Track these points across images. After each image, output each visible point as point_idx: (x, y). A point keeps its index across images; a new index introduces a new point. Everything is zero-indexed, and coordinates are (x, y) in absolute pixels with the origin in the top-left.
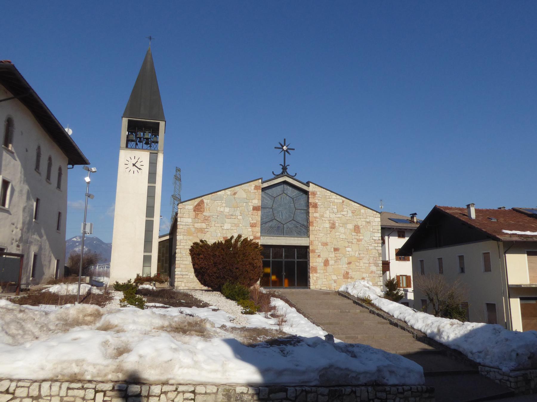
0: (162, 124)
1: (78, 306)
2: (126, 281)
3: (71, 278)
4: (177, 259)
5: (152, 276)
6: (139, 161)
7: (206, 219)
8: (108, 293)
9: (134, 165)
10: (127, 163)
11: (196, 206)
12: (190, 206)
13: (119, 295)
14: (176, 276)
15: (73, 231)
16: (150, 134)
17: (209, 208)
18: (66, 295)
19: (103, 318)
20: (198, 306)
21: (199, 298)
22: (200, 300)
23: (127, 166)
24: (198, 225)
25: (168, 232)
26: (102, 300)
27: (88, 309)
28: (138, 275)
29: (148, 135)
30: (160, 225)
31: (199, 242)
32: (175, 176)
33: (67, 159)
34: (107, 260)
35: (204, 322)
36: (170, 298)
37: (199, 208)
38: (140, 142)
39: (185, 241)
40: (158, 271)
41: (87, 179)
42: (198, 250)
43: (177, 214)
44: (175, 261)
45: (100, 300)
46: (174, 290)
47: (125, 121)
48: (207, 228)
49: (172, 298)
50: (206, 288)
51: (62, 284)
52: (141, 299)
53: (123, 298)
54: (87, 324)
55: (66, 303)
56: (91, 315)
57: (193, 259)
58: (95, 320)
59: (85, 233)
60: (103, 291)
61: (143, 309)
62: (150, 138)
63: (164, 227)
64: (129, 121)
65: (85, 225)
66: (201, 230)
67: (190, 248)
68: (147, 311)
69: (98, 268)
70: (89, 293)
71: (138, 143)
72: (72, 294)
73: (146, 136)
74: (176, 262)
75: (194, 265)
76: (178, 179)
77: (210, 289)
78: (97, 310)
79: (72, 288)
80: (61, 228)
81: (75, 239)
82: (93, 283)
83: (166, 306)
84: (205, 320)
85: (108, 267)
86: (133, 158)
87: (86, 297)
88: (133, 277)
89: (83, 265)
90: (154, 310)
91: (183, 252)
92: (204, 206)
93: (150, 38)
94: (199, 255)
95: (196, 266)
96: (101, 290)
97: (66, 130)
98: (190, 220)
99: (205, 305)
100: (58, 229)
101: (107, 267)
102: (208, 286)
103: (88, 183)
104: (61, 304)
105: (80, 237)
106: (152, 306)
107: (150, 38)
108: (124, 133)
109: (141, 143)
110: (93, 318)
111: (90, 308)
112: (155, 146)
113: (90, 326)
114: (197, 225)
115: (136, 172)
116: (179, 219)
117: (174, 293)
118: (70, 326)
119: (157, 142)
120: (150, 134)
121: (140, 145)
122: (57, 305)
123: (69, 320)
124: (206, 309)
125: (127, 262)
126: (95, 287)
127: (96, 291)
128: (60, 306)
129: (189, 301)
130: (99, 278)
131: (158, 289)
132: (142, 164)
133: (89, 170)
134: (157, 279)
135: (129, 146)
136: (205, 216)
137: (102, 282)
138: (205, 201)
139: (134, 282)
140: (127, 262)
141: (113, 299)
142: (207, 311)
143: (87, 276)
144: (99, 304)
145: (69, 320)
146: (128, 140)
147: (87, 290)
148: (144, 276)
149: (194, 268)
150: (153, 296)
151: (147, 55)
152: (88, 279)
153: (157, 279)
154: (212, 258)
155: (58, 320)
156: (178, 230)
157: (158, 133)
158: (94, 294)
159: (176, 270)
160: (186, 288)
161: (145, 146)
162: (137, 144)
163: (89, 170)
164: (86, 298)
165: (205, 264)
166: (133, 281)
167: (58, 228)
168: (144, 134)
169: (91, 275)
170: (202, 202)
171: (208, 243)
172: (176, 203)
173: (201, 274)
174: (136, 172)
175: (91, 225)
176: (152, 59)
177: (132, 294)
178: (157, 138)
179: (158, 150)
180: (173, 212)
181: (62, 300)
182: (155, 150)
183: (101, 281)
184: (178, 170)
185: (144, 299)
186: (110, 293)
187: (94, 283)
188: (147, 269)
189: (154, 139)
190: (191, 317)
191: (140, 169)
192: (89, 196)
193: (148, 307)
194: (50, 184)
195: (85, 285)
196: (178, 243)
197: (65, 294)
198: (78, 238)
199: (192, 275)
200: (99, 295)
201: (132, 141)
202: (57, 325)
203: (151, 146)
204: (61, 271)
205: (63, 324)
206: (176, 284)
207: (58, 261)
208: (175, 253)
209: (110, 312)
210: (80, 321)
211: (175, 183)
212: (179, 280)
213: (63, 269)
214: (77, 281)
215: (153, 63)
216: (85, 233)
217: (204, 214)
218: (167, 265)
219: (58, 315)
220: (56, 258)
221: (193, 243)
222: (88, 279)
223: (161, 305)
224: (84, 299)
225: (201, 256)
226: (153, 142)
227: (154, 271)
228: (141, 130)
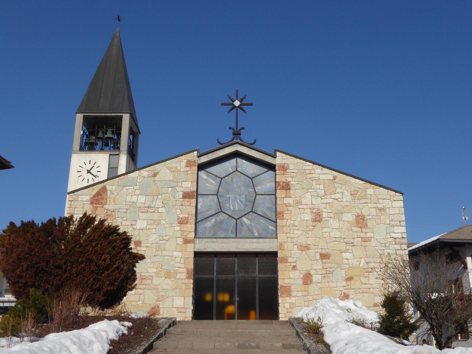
6: (95, 166)
9: (89, 172)
10: (80, 169)
11: (95, 196)
17: (115, 198)
23: (80, 174)
47: (79, 118)
86: (87, 163)
92: (107, 195)
93: (119, 19)
107: (119, 19)
132: (99, 169)
136: (108, 210)
138: (109, 188)
170: (104, 189)
191: (95, 176)
217: (106, 207)
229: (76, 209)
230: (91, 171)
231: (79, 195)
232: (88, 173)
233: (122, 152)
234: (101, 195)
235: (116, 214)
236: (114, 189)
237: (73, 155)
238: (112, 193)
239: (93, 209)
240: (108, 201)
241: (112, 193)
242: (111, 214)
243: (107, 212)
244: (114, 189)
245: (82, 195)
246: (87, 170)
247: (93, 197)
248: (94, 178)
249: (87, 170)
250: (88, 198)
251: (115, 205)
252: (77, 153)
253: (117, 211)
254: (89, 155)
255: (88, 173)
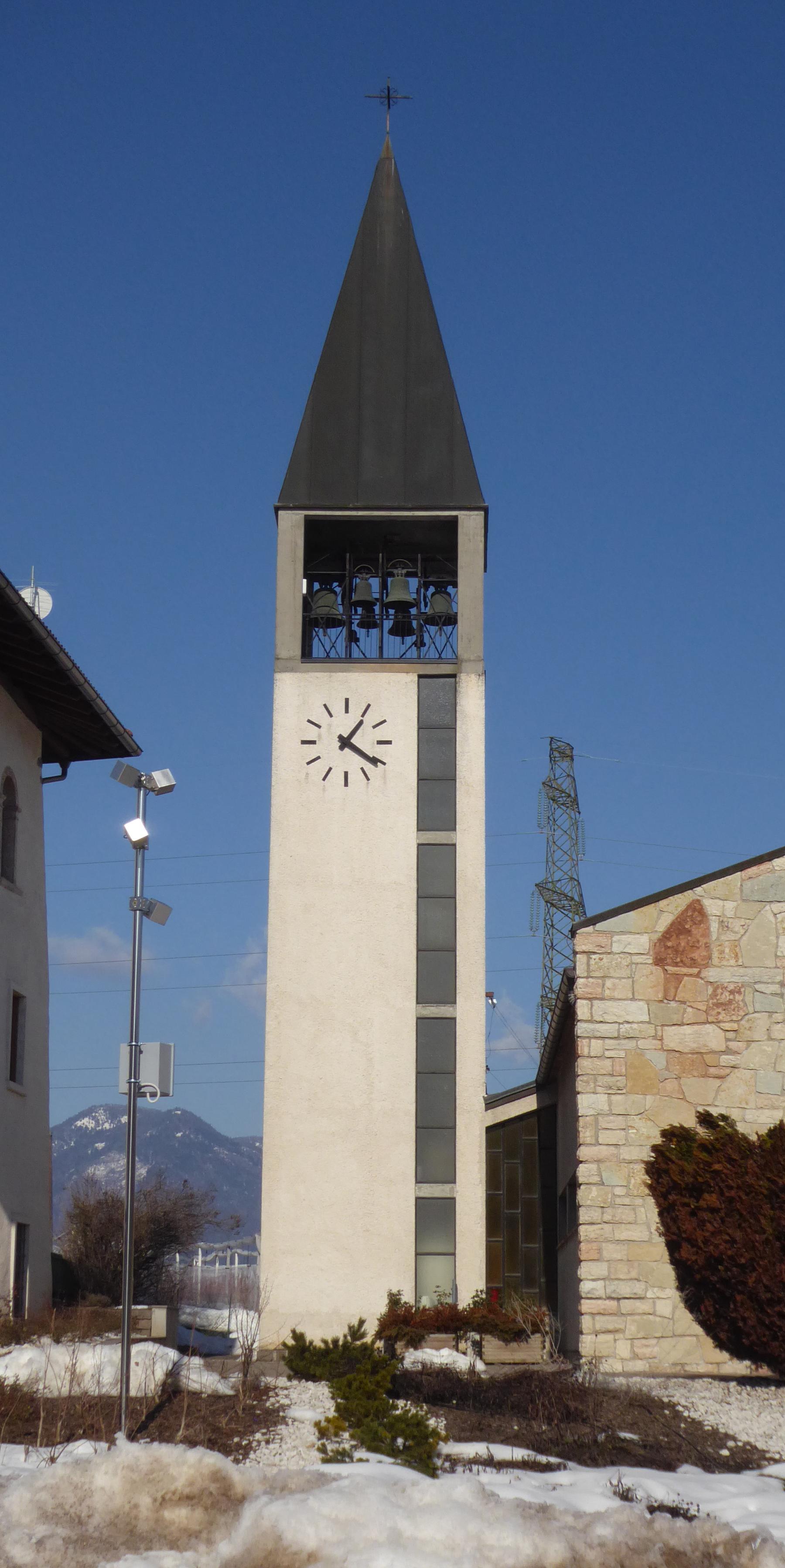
0: (470, 524)
1: (130, 1452)
2: (338, 1331)
3: (84, 1310)
4: (584, 1215)
5: (465, 1301)
6: (371, 719)
7: (723, 1004)
8: (261, 1392)
9: (345, 743)
10: (311, 733)
11: (667, 935)
12: (632, 937)
13: (310, 1403)
14: (586, 1306)
15: (83, 1081)
16: (414, 583)
17: (735, 944)
18: (70, 1398)
19: (249, 1513)
20: (711, 1464)
21: (710, 1422)
22: (715, 1432)
23: (311, 751)
24: (681, 1037)
25: (530, 1075)
26: (234, 1423)
27: (173, 1471)
28: (394, 1300)
29: (405, 588)
30: (489, 1036)
31: (690, 1122)
32: (550, 787)
33: (37, 736)
34: (242, 1224)
35: (746, 1552)
36: (564, 1417)
37: (680, 948)
38: (368, 623)
39: (620, 1121)
40: (491, 1275)
41: (136, 830)
42: (690, 1168)
43: (570, 981)
44: (574, 1223)
45: (223, 1421)
46: (579, 1376)
47: (291, 527)
48: (728, 1051)
49: (570, 1416)
50: (742, 1367)
51: (46, 1340)
52: (420, 1423)
53: (332, 1413)
54: (174, 1545)
55: (70, 1438)
56: (188, 1499)
57: (666, 1212)
58: (211, 1524)
59: (136, 1091)
60: (236, 1378)
61: (432, 1472)
62: (416, 604)
63: (506, 1043)
64: (311, 525)
65: (136, 1053)
66: (701, 1063)
67: (648, 1155)
68: (457, 1487)
69: (201, 1266)
70: (172, 1388)
71: (361, 633)
72: (94, 1391)
73: (395, 595)
74: (584, 1231)
75: (673, 1247)
76: (562, 798)
77: (765, 1371)
78: (218, 1477)
79: (86, 1365)
80: (28, 1068)
81: (87, 1122)
82: (191, 1340)
83: (543, 1459)
84: (751, 1538)
85: (250, 1260)
86: (337, 708)
87: (159, 1408)
88: (374, 1310)
89: (137, 1250)
90: (488, 1477)
91: (614, 1177)
92: (707, 933)
93: (388, 98)
94: (696, 1190)
95: (686, 1252)
96: (224, 1376)
97: (26, 594)
98: (638, 1011)
99: (746, 1460)
100: (13, 1076)
101: (244, 1260)
102: (756, 1358)
103: (141, 846)
104: (50, 1442)
105: (113, 1113)
106: (476, 1461)
107: (388, 98)
108: (291, 585)
109: (374, 632)
110: (199, 1514)
111: (187, 1463)
112: (440, 641)
113: (189, 1555)
114: (675, 1037)
115: (356, 777)
116: (582, 1009)
117: (582, 1392)
118: (96, 1551)
119: (451, 620)
120: (414, 583)
121: (368, 640)
122: (33, 1443)
123: (96, 1520)
124: (748, 1478)
125: (340, 1233)
126: (196, 1361)
127: (200, 1377)
128: (45, 1452)
129: (664, 1438)
130: (212, 1313)
131: (500, 1372)
132: (383, 733)
133: (139, 784)
134: (481, 1321)
135: (317, 650)
136: (717, 987)
137: (225, 1335)
138: (712, 907)
139: (379, 1335)
140: (340, 1233)
141: (284, 1421)
142: (758, 1492)
143: (156, 1301)
144: (218, 1442)
145: (96, 1520)
146: (311, 623)
147: (160, 1374)
148: (426, 1302)
149: (675, 1261)
150: (483, 1406)
151: (375, 181)
152: (159, 1316)
153: (481, 1321)
154: (767, 1209)
155: (45, 1516)
156: (583, 1066)
157: (454, 573)
158: (195, 1395)
159: (584, 1271)
160: (640, 1366)
161: (394, 645)
162: (353, 638)
163: (139, 784)
164: (160, 1416)
165: (733, 1241)
166: (371, 1328)
167: (14, 1074)
168: (384, 586)
169: (171, 1297)
170: (696, 911)
171: (741, 1128)
172: (564, 923)
173: (712, 1291)
174: (356, 777)
175: (165, 1051)
176: (400, 199)
177: (371, 1396)
178: (450, 599)
179: (456, 660)
180: (549, 968)
181: (51, 1419)
182: (440, 659)
183: (223, 1327)
184: (561, 752)
185: (432, 1422)
186: (267, 1389)
187: (192, 1339)
188: (436, 1267)
189: (438, 606)
190: (680, 1522)
191: (374, 761)
192: (146, 913)
193: (454, 1462)
194: (20, 893)
195: (150, 1347)
196: (585, 1134)
197: (65, 1391)
198: (101, 1115)
199: (666, 1298)
200: (216, 1397)
201: (332, 622)
202: (40, 1543)
203: (420, 644)
204: (40, 1278)
205: (67, 1541)
206: (587, 1345)
207: (22, 1230)
208: (574, 1185)
209: (278, 1488)
210: (143, 1527)
211: (552, 821)
212: (602, 1322)
213: (47, 1268)
214: (115, 1327)
215: (408, 219)
216: (136, 1091)
217: (711, 974)
218: (537, 1246)
219: (44, 1496)
220: (11, 1220)
221: (664, 1134)
222: (159, 1316)
223: (520, 1454)
224: (151, 1417)
225: (711, 1199)
226: (432, 620)
227: (470, 1280)
228: (367, 564)
229: (609, 983)
230: (354, 741)
231: (612, 933)
232: (342, 748)
233: (465, 666)
234: (689, 932)
235: (749, 999)
236: (730, 913)
237: (278, 676)
238: (724, 925)
239: (666, 979)
240: (715, 955)
241: (724, 925)
242: (730, 1002)
243: (714, 995)
244: (730, 913)
245: (623, 933)
246: (341, 737)
247: (660, 940)
248: (368, 767)
249: (341, 737)
250: (642, 943)
251: (742, 971)
252: (292, 670)
253: (749, 990)
254: (341, 676)
255: (342, 748)
